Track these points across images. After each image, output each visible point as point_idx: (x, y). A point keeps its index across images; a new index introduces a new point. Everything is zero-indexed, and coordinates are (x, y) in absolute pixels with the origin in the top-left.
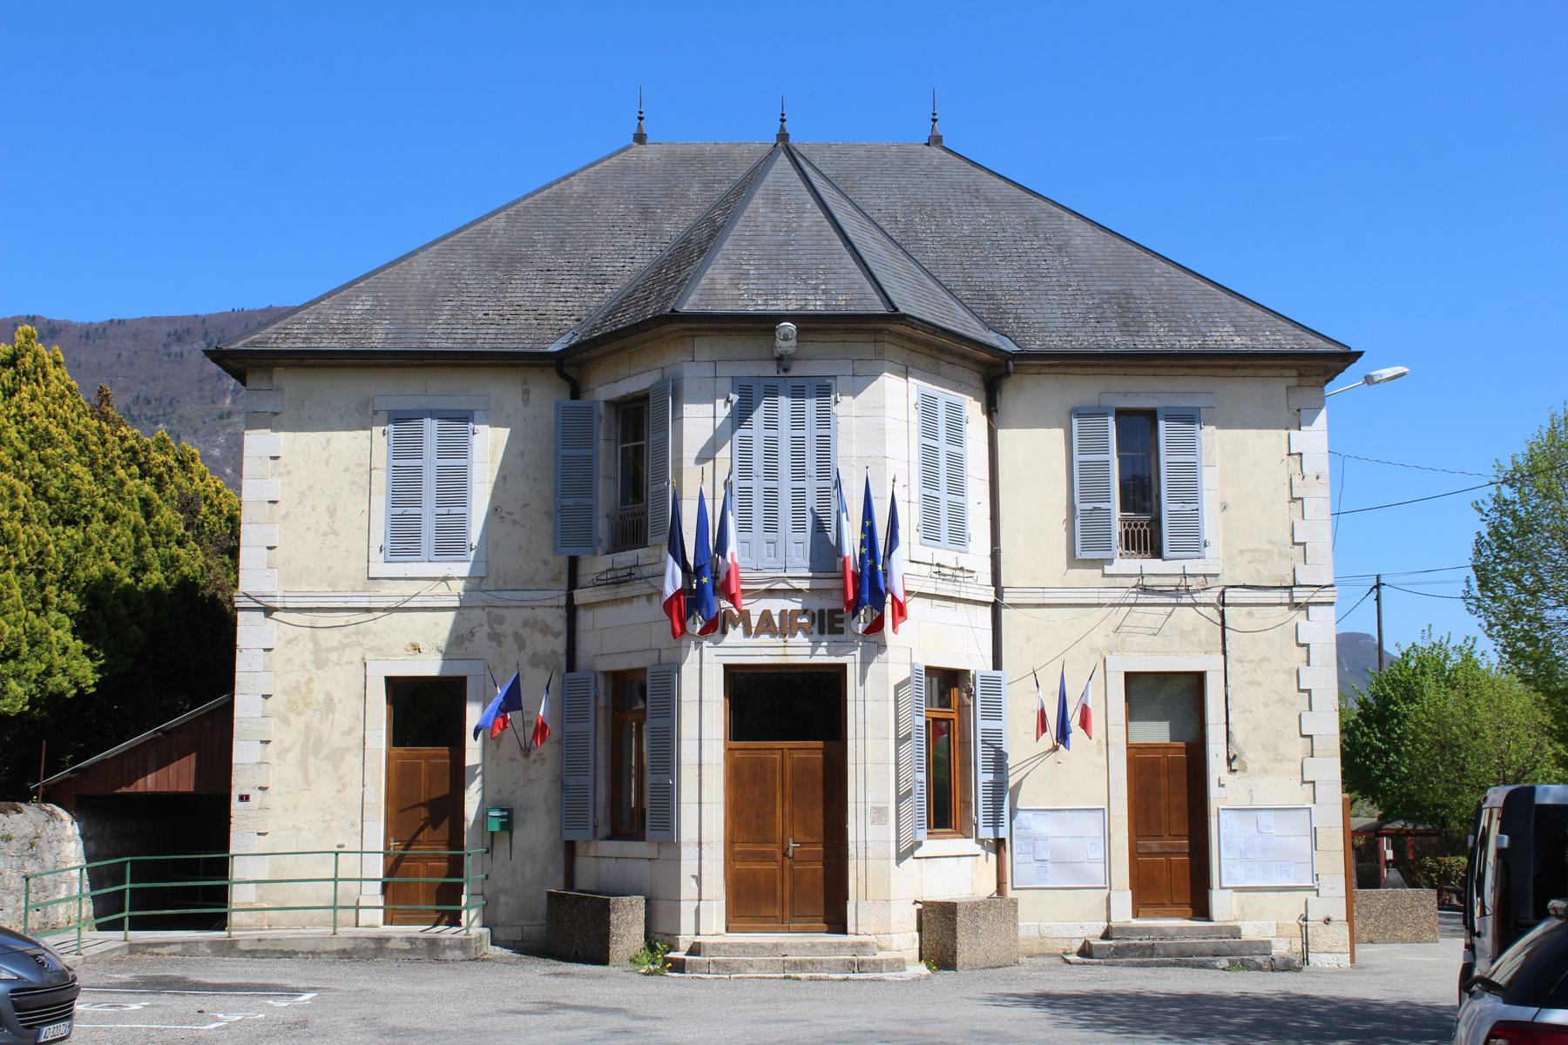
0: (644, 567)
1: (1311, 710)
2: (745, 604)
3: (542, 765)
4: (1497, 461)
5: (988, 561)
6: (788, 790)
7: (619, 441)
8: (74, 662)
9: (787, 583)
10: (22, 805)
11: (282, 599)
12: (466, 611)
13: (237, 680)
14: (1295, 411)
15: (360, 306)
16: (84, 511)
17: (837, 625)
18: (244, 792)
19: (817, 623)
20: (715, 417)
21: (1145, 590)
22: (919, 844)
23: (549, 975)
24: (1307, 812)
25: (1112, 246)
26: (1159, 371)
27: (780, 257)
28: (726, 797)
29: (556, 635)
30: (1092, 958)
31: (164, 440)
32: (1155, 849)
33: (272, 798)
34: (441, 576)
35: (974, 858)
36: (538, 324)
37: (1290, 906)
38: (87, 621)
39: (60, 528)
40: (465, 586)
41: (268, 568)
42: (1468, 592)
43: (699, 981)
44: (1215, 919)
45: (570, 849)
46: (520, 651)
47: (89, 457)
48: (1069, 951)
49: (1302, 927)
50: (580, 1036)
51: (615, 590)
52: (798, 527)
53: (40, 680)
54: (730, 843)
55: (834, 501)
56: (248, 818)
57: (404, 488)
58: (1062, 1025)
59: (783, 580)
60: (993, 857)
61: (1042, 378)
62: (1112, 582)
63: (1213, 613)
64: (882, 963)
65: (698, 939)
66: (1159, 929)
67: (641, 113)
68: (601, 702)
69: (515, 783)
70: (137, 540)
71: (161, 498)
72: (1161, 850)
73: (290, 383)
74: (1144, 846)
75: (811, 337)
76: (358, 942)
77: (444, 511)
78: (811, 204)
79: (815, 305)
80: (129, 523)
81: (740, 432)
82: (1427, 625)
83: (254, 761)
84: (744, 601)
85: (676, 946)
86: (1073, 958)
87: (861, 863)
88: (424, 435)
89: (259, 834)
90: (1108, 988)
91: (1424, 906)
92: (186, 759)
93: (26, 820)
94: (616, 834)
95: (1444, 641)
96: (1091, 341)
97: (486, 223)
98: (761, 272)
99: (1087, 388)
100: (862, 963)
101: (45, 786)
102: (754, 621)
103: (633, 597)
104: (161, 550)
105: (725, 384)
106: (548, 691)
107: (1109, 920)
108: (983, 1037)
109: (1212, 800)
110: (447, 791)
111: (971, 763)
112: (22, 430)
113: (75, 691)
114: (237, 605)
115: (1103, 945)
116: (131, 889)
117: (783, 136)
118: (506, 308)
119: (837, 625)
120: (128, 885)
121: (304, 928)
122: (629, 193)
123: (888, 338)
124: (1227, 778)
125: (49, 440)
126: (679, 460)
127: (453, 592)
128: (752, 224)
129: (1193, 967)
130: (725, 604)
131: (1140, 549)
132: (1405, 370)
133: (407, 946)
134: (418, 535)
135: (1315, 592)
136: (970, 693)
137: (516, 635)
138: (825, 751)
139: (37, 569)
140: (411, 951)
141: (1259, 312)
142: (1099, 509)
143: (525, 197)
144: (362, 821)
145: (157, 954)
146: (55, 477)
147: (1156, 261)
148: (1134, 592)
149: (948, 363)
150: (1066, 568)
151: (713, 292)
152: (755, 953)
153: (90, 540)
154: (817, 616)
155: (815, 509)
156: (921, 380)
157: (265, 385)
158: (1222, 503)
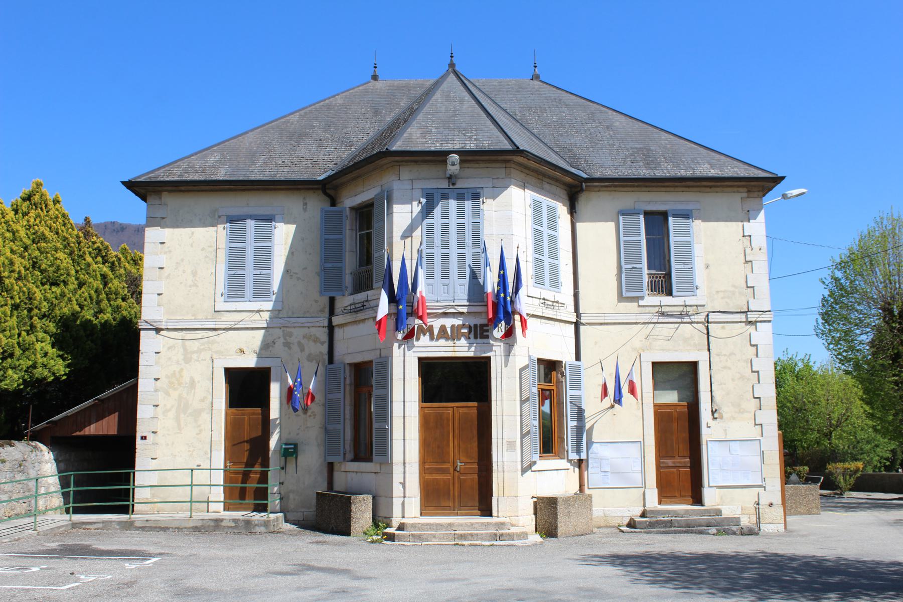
0: (372, 302)
1: (759, 383)
2: (430, 321)
3: (314, 418)
4: (832, 257)
5: (572, 298)
6: (457, 431)
7: (358, 231)
8: (51, 361)
9: (455, 309)
10: (16, 442)
11: (166, 324)
12: (271, 330)
13: (140, 370)
14: (746, 211)
15: (212, 159)
16: (62, 278)
17: (485, 334)
18: (144, 435)
19: (473, 333)
20: (412, 212)
21: (663, 314)
22: (535, 463)
23: (313, 543)
24: (758, 441)
25: (637, 126)
26: (668, 189)
27: (450, 123)
28: (420, 436)
29: (322, 343)
30: (636, 529)
31: (125, 249)
32: (671, 464)
33: (159, 438)
34: (256, 309)
35: (566, 471)
36: (313, 166)
37: (750, 496)
38: (61, 338)
39: (47, 287)
40: (270, 315)
41: (158, 306)
42: (817, 326)
43: (402, 547)
44: (706, 504)
45: (331, 467)
46: (301, 352)
47: (70, 250)
48: (622, 524)
49: (756, 509)
50: (310, 596)
51: (355, 316)
52: (462, 276)
53: (29, 370)
54: (422, 463)
55: (482, 261)
56: (146, 449)
57: (235, 259)
58: (636, 581)
59: (453, 307)
60: (577, 470)
61: (600, 193)
62: (643, 310)
63: (702, 327)
64: (514, 535)
65: (403, 521)
66: (674, 511)
67: (375, 64)
68: (348, 382)
69: (299, 429)
70: (98, 296)
71: (113, 275)
72: (673, 465)
73: (172, 201)
74: (663, 463)
75: (466, 165)
76: (204, 522)
77: (258, 272)
78: (467, 97)
79: (470, 146)
80: (93, 287)
81: (426, 221)
82: (785, 348)
83: (149, 417)
84: (429, 320)
85: (391, 524)
86: (625, 529)
87: (500, 474)
88: (247, 231)
89: (152, 459)
90: (653, 550)
91: (812, 495)
92: (113, 415)
93: (17, 450)
94: (357, 459)
95: (794, 357)
96: (629, 172)
97: (288, 118)
98: (439, 130)
99: (627, 199)
100: (502, 535)
101: (31, 431)
102: (436, 332)
103: (365, 319)
104: (112, 303)
105: (418, 193)
106: (316, 375)
107: (644, 506)
108: (587, 593)
109: (703, 435)
110: (260, 433)
111: (564, 415)
112: (29, 233)
113: (52, 378)
114: (140, 327)
115: (642, 521)
116: (74, 491)
117: (452, 65)
118: (295, 159)
119: (485, 334)
120: (72, 489)
121: (178, 513)
122: (368, 103)
123: (513, 166)
124: (712, 423)
125: (44, 239)
126: (391, 237)
127: (263, 319)
128: (434, 107)
129: (696, 533)
130: (418, 322)
131: (659, 291)
132: (804, 190)
133: (233, 524)
134: (243, 286)
135: (760, 315)
136: (563, 374)
137: (299, 343)
138: (478, 408)
139: (29, 307)
140: (235, 527)
141: (723, 157)
142: (636, 268)
143: (310, 106)
144: (211, 451)
145: (88, 529)
146: (46, 259)
147: (663, 133)
148: (656, 316)
149: (548, 183)
150: (617, 302)
151: (410, 140)
152: (437, 529)
153: (64, 293)
154: (473, 329)
155: (472, 265)
156: (532, 191)
157: (157, 202)
158: (706, 264)
